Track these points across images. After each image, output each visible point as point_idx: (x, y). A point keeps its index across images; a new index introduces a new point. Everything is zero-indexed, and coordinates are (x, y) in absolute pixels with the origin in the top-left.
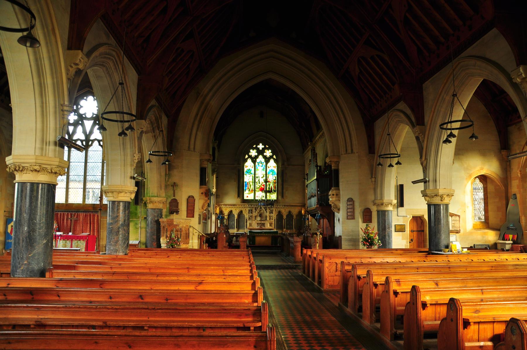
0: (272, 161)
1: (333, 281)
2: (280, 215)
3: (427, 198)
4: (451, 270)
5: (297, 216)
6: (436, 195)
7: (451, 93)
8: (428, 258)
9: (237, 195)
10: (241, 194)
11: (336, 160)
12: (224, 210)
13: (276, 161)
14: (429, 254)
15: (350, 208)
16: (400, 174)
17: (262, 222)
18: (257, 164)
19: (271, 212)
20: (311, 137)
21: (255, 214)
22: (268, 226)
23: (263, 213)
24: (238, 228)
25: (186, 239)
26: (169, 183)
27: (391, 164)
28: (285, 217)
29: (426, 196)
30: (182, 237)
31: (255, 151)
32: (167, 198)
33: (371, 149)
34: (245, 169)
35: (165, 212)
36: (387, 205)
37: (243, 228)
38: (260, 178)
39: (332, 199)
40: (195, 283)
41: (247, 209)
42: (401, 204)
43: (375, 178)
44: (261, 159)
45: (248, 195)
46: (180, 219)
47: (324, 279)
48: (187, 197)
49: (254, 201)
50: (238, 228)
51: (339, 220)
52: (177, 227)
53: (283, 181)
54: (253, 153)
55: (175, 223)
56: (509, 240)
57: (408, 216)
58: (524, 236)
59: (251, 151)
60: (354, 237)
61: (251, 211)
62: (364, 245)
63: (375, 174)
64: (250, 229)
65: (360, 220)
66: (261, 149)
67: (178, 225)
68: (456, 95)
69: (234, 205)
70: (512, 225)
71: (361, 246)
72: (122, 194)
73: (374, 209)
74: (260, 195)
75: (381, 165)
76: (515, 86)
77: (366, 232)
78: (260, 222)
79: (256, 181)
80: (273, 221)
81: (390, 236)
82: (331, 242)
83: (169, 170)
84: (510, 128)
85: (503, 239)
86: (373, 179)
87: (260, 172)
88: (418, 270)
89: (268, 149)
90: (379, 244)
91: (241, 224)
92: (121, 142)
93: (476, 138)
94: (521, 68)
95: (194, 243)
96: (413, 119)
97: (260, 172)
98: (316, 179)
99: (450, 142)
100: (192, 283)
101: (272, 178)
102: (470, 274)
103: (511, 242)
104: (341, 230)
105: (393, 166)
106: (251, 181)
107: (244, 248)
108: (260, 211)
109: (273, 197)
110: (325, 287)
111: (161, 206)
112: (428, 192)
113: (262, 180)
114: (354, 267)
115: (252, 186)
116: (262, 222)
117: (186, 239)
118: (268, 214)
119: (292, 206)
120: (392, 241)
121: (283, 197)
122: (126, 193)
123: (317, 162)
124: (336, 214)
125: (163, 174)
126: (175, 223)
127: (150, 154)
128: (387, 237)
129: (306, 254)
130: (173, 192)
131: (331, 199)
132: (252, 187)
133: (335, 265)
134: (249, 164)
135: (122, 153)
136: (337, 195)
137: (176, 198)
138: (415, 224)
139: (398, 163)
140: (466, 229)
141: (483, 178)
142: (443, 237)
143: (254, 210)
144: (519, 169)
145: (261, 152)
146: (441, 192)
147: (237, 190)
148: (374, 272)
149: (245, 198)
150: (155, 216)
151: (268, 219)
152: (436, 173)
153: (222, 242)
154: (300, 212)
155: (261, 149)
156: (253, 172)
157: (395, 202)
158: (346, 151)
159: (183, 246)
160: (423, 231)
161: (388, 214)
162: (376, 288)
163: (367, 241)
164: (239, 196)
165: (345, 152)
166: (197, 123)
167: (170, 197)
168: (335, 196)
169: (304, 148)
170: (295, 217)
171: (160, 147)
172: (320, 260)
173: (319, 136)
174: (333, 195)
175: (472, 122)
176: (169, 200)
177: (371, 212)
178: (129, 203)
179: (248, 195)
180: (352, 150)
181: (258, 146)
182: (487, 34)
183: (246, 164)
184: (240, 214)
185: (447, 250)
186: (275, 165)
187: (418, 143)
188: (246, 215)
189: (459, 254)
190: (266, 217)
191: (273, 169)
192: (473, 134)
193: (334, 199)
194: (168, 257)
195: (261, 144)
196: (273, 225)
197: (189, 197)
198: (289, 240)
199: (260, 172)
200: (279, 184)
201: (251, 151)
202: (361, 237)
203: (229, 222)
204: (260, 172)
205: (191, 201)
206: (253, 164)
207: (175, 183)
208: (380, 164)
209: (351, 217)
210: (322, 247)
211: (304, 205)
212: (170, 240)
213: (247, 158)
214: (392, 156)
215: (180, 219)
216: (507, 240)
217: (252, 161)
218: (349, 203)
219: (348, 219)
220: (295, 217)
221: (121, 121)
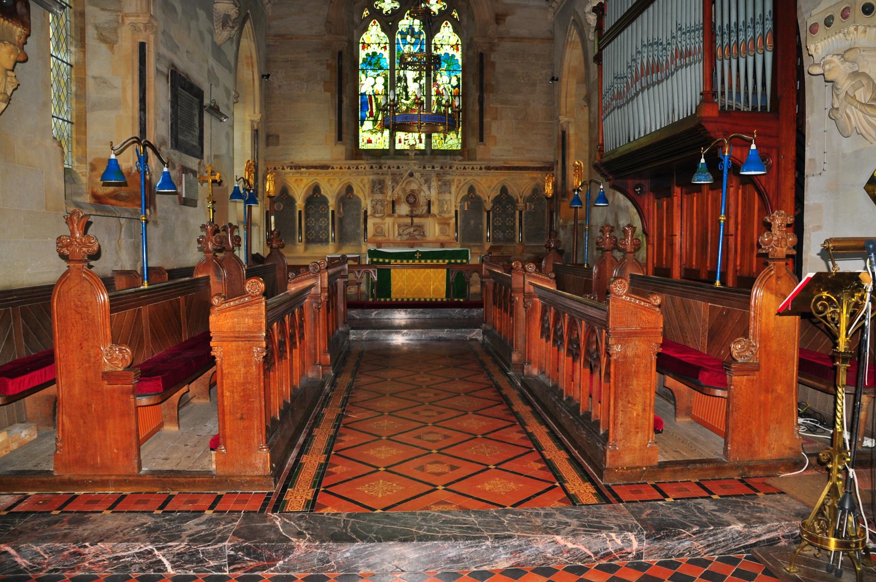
2: (472, 198)
9: (333, 135)
17: (416, 220)
19: (445, 186)
22: (433, 230)
38: (410, 82)
53: (352, 54)
61: (378, 186)
84: (34, 426)
118: (433, 194)
143: (389, 183)
147: (334, 118)
149: (363, 145)
179: (372, 137)
183: (366, 37)
184: (347, 196)
186: (455, 39)
190: (429, 204)
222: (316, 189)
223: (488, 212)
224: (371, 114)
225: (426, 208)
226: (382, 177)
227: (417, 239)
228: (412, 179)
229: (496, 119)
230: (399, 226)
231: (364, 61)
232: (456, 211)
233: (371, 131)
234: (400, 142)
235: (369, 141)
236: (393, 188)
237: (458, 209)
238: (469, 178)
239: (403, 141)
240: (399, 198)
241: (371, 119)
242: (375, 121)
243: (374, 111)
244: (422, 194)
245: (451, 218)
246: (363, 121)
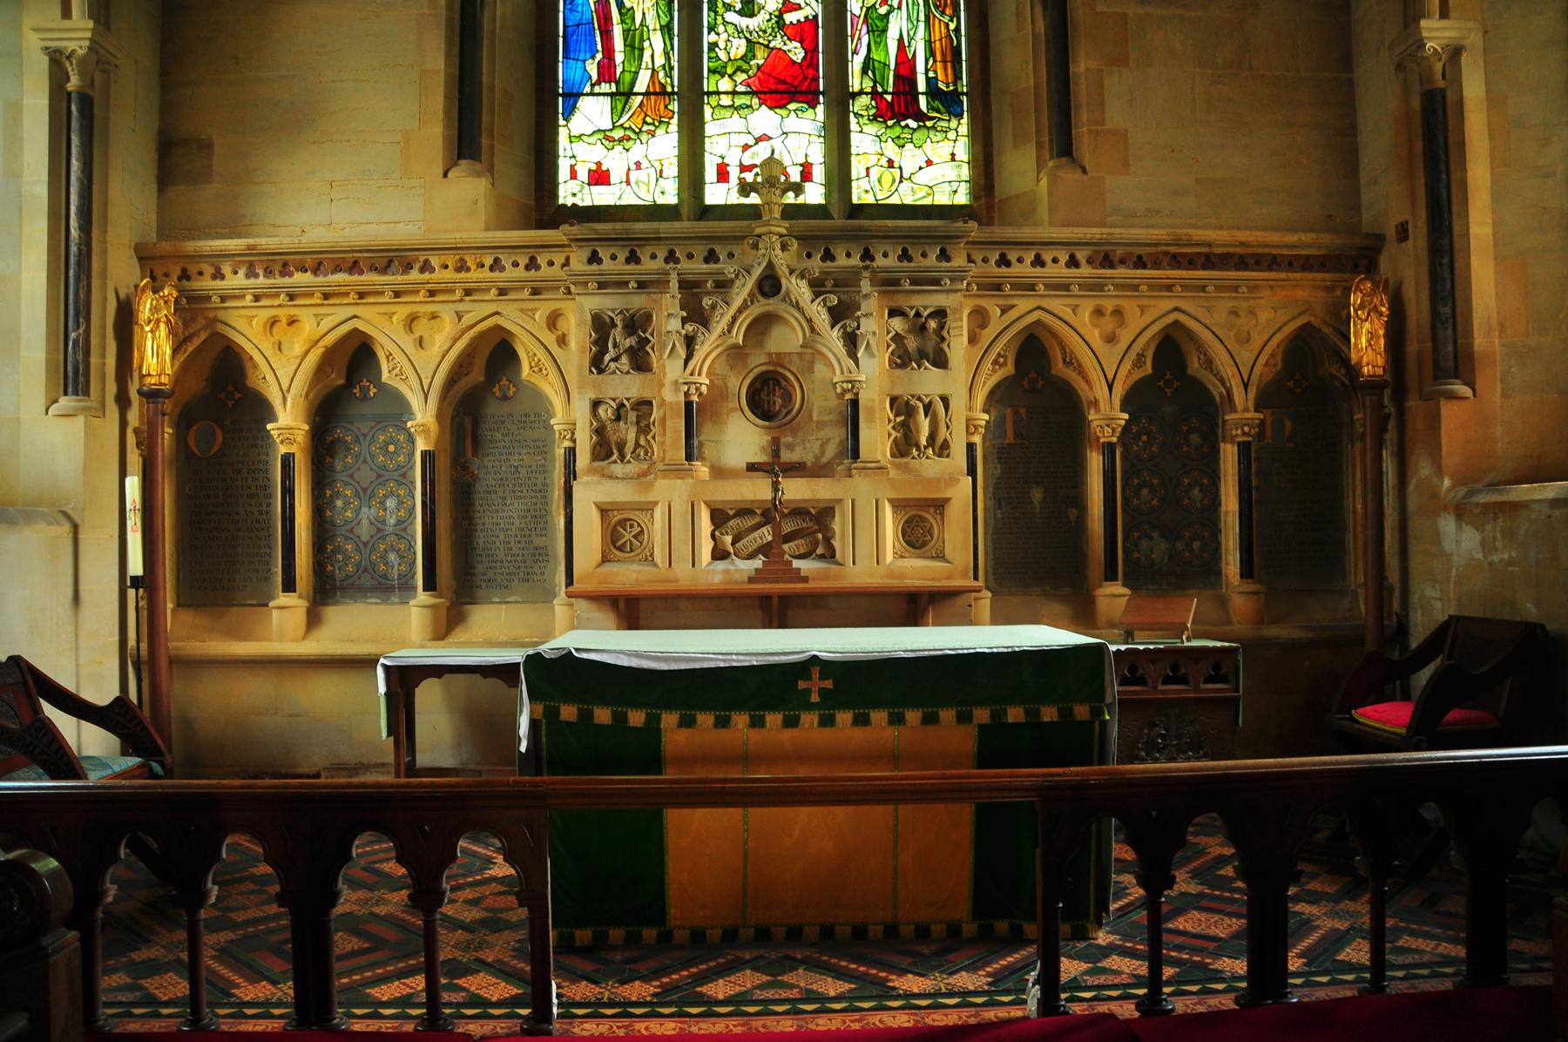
2: (1036, 389)
9: (435, 133)
12: (248, 329)
17: (796, 490)
19: (922, 347)
21: (673, 378)
23: (811, 351)
28: (1107, 416)
37: (528, 574)
45: (616, 162)
61: (622, 341)
69: (391, 259)
78: (759, 490)
91: (499, 521)
108: (762, 325)
109: (929, 168)
116: (796, 490)
118: (873, 374)
119: (1210, 261)
143: (669, 320)
149: (570, 192)
151: (877, 438)
170: (1243, 412)
179: (610, 157)
188: (562, 390)
190: (852, 414)
203: (344, 508)
223: (1108, 450)
224: (607, 71)
225: (836, 436)
226: (638, 302)
227: (797, 576)
228: (772, 305)
229: (1120, 61)
230: (719, 517)
232: (971, 447)
233: (606, 137)
234: (723, 175)
235: (599, 177)
236: (690, 342)
237: (977, 439)
238: (1024, 304)
239: (734, 173)
240: (718, 394)
241: (605, 88)
242: (623, 95)
243: (619, 57)
244: (820, 369)
245: (952, 481)
246: (573, 97)
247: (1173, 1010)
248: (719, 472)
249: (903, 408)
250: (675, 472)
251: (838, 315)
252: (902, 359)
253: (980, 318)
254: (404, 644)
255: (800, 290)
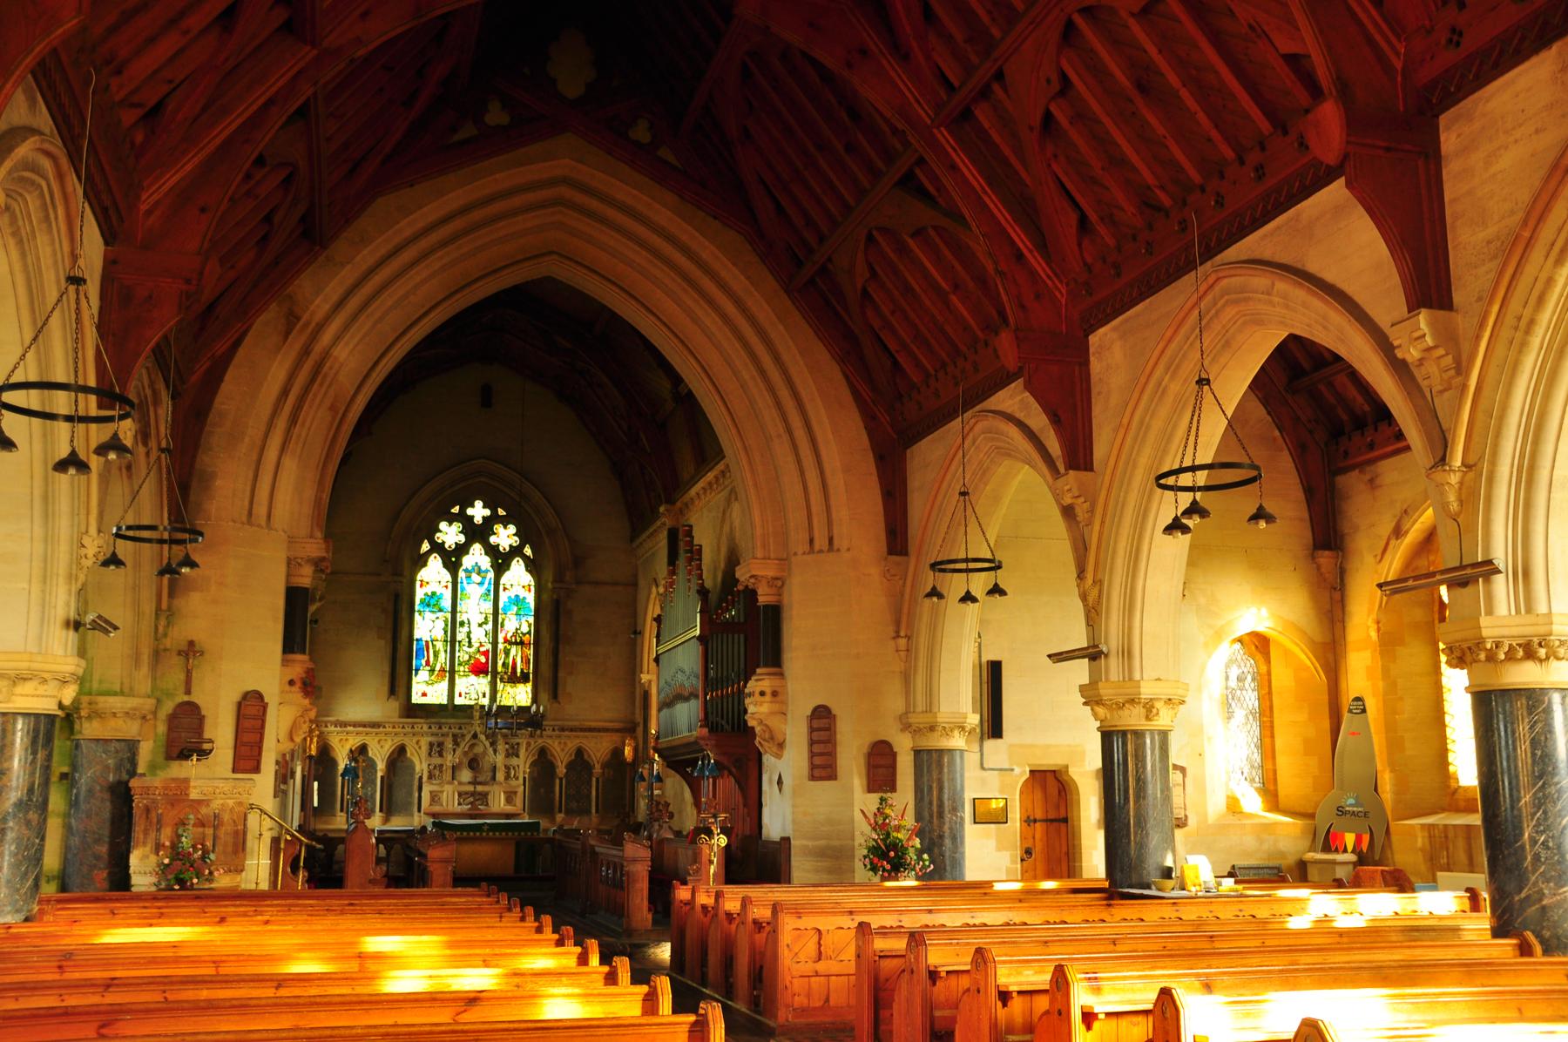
0: (518, 566)
1: (808, 996)
2: (543, 762)
3: (1101, 711)
4: (1217, 945)
5: (605, 766)
6: (1132, 701)
7: (1189, 370)
8: (1114, 910)
9: (385, 689)
10: (401, 682)
11: (771, 574)
13: (532, 566)
14: (1111, 897)
15: (819, 742)
16: (1027, 626)
17: (480, 788)
18: (461, 574)
19: (513, 752)
20: (673, 488)
21: (450, 759)
22: (498, 803)
23: (485, 753)
24: (389, 809)
25: (235, 852)
26: (168, 642)
27: (968, 592)
28: (561, 770)
29: (1099, 702)
30: (219, 848)
31: (457, 527)
32: (159, 701)
33: (897, 540)
34: (420, 594)
35: (146, 752)
36: (947, 732)
37: (405, 809)
39: (757, 710)
40: (454, 1000)
41: (424, 742)
42: (994, 726)
43: (908, 637)
44: (476, 556)
45: (428, 689)
46: (210, 779)
47: (781, 986)
48: (236, 697)
49: (450, 711)
50: (389, 809)
51: (780, 782)
52: (204, 810)
53: (557, 639)
54: (450, 534)
55: (194, 795)
56: (1345, 851)
57: (1017, 770)
58: (1394, 838)
59: (443, 525)
60: (836, 843)
61: (437, 749)
62: (874, 869)
63: (910, 625)
64: (434, 815)
65: (858, 782)
66: (478, 520)
67: (206, 803)
68: (1208, 382)
70: (1351, 801)
71: (861, 873)
72: (28, 687)
73: (904, 747)
74: (473, 689)
75: (940, 596)
76: (1400, 368)
77: (881, 824)
78: (471, 788)
79: (459, 638)
80: (518, 785)
81: (957, 839)
82: (756, 861)
83: (171, 595)
84: (1341, 480)
85: (1327, 848)
86: (902, 642)
87: (474, 605)
88: (1118, 948)
89: (505, 522)
90: (924, 867)
91: (399, 795)
92: (37, 493)
93: (1270, 519)
94: (1421, 317)
95: (258, 870)
96: (1054, 446)
97: (475, 606)
98: (700, 638)
99: (1185, 529)
100: (442, 1000)
101: (518, 623)
102: (1287, 958)
103: (1352, 857)
104: (789, 817)
105: (974, 600)
106: (439, 634)
107: (443, 886)
108: (473, 746)
109: (519, 696)
110: (784, 1016)
111: (130, 729)
112: (1105, 691)
113: (480, 636)
114: (916, 939)
115: (442, 656)
116: (480, 788)
117: (235, 852)
118: (500, 759)
119: (591, 730)
120: (963, 854)
121: (555, 696)
122: (45, 681)
123: (700, 577)
124: (768, 760)
125: (148, 608)
126: (194, 795)
127: (118, 535)
128: (947, 842)
129: (690, 903)
130: (182, 677)
131: (751, 709)
132: (443, 659)
133: (816, 938)
134: (433, 575)
135: (38, 530)
136: (775, 694)
137: (195, 697)
138: (1039, 795)
139: (996, 590)
140: (1205, 815)
141: (1259, 644)
142: (1154, 839)
143: (449, 745)
144: (1374, 616)
145: (477, 533)
146: (1147, 690)
147: (386, 668)
148: (998, 954)
149: (416, 699)
150: (107, 767)
151: (500, 776)
152: (1130, 628)
153: (362, 866)
154: (617, 752)
155: (478, 520)
156: (446, 603)
157: (974, 719)
158: (811, 541)
159: (223, 881)
160: (1065, 820)
161: (952, 763)
162: (1005, 1005)
163: (884, 855)
164: (392, 692)
165: (807, 548)
166: (281, 424)
167: (170, 695)
168: (768, 698)
169: (638, 520)
170: (597, 769)
171: (149, 508)
172: (755, 922)
173: (701, 484)
174: (762, 694)
175: (1257, 468)
176: (168, 707)
177: (894, 755)
178: (51, 718)
179: (427, 689)
180: (831, 540)
181: (470, 511)
182: (1310, 200)
183: (423, 574)
184: (398, 757)
185: (1170, 883)
186: (528, 579)
187: (1069, 528)
188: (420, 763)
189: (1210, 897)
190: (494, 769)
191: (523, 593)
192: (1261, 508)
193: (765, 709)
194: (222, 920)
195: (479, 504)
196: (519, 800)
197: (246, 696)
198: (594, 854)
199: (474, 605)
200: (543, 651)
201: (443, 525)
202: (859, 840)
204: (475, 606)
205: (251, 710)
206: (446, 576)
207: (191, 643)
208: (935, 593)
209: (824, 773)
210: (722, 878)
211: (633, 727)
212: (172, 860)
213: (429, 553)
214: (972, 565)
215: (210, 779)
216: (1337, 851)
217: (446, 565)
218: (816, 724)
219: (813, 778)
220: (597, 769)
221: (69, 419)
222: (363, 749)
224: (428, 663)
231: (422, 602)
235: (424, 695)
247: (317, 563)
248: (460, 783)
249: (507, 768)
250: (450, 783)
251: (492, 744)
252: (508, 755)
253: (529, 744)
254: (1369, 636)
255: (483, 737)
